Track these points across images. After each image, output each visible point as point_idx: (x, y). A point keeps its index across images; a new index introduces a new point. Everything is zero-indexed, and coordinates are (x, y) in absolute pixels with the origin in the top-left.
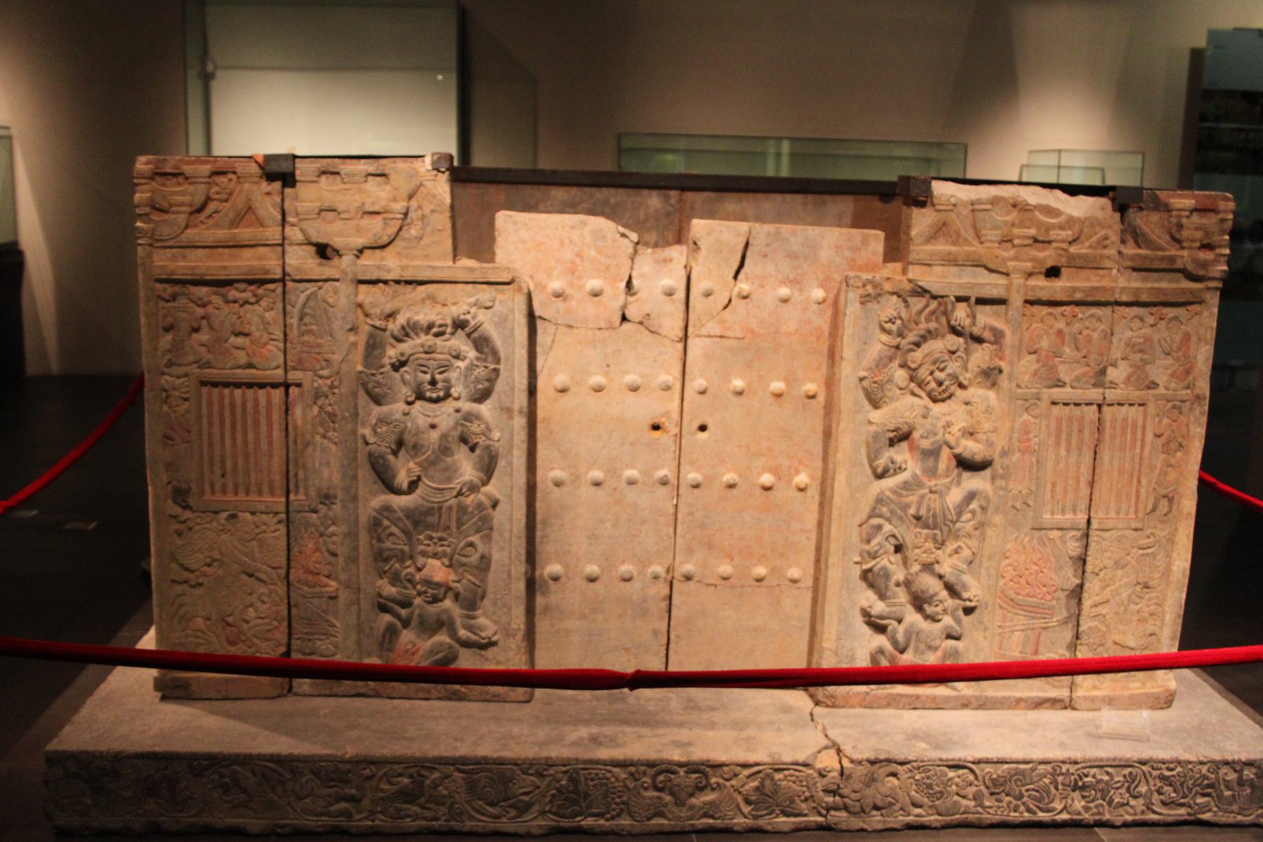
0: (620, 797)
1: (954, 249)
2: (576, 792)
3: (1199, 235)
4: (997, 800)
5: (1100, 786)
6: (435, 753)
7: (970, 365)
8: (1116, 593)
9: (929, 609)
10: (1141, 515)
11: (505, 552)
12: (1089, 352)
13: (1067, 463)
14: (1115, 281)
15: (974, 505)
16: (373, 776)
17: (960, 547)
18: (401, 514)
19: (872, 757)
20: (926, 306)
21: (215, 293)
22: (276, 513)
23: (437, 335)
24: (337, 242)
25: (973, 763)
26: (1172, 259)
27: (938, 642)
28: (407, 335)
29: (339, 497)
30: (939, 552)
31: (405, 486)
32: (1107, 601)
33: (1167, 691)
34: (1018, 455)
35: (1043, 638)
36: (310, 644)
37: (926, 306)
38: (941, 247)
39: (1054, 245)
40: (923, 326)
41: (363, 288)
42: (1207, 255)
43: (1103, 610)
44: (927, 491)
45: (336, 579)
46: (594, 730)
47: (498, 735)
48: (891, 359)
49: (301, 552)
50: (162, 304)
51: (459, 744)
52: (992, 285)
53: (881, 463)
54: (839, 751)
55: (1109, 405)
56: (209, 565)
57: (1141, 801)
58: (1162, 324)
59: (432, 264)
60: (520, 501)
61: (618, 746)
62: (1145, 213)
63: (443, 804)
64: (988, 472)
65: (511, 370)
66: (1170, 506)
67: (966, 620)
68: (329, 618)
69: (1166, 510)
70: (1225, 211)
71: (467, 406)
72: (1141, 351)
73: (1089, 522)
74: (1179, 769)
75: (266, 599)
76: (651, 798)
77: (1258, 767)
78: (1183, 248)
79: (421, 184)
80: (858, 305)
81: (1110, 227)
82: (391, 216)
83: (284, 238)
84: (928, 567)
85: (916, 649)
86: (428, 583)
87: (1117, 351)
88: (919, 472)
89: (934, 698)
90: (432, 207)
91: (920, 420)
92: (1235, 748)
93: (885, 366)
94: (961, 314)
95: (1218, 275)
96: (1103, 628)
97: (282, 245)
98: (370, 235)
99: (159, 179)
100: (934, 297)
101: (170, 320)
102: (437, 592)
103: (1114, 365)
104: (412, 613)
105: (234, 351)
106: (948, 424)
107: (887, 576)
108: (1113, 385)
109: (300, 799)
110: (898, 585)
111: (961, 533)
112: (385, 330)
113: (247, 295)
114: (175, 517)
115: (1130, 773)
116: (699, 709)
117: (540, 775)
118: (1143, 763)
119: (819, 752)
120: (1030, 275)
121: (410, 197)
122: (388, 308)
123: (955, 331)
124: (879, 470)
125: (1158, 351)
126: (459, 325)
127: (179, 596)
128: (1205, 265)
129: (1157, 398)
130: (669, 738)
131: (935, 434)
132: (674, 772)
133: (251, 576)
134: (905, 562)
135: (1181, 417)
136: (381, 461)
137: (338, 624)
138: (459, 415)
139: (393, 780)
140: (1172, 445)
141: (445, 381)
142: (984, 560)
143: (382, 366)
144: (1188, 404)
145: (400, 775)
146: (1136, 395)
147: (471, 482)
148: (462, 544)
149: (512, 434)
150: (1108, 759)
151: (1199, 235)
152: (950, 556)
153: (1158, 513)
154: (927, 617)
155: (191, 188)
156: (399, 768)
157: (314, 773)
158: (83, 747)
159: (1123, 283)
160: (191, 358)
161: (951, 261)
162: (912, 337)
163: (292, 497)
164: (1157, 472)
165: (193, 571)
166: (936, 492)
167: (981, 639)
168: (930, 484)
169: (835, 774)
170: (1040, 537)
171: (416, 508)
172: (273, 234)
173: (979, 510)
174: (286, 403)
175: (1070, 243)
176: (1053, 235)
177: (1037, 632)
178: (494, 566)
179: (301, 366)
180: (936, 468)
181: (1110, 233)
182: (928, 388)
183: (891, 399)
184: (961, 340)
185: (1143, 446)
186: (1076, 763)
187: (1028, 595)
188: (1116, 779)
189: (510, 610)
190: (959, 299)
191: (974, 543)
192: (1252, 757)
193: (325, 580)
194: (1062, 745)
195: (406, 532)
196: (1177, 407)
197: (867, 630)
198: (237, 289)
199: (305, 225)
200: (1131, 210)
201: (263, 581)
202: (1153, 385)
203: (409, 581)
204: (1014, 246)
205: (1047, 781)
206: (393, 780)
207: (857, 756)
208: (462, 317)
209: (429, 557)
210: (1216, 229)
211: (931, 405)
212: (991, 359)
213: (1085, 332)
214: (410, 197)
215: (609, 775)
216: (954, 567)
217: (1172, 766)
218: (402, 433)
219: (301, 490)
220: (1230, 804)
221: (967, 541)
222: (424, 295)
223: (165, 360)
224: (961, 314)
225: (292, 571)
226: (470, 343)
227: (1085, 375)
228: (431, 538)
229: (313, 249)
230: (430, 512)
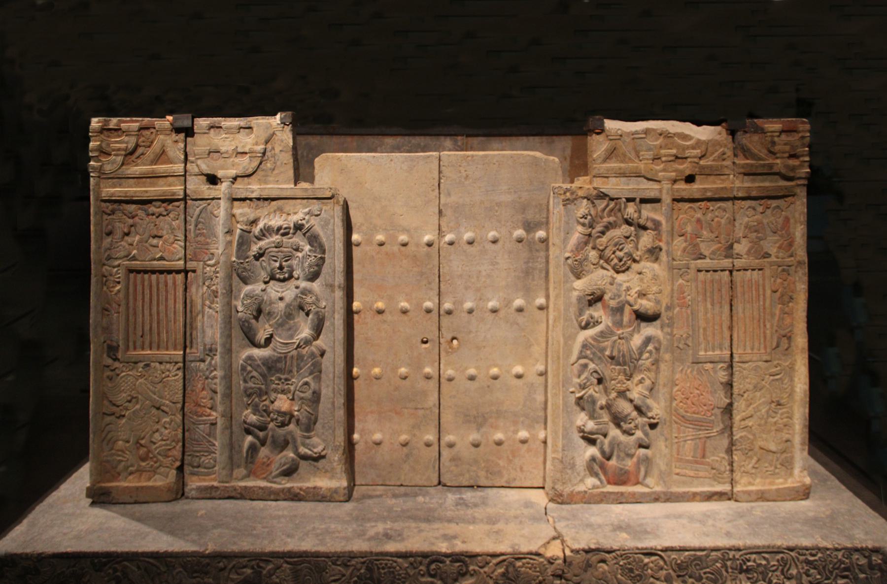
1: (622, 165)
3: (787, 148)
6: (269, 549)
7: (639, 246)
8: (757, 410)
9: (625, 426)
11: (331, 390)
12: (720, 233)
14: (733, 183)
17: (643, 378)
18: (259, 362)
20: (607, 206)
22: (176, 363)
23: (283, 235)
24: (220, 174)
25: (662, 551)
26: (771, 166)
27: (633, 451)
28: (264, 235)
30: (628, 382)
31: (263, 341)
32: (751, 416)
34: (678, 309)
35: (708, 444)
36: (197, 459)
37: (607, 206)
38: (613, 165)
39: (689, 160)
41: (236, 203)
42: (793, 162)
43: (750, 423)
44: (617, 337)
46: (389, 525)
47: (318, 531)
49: (193, 391)
50: (105, 217)
51: (289, 540)
52: (649, 189)
54: (563, 542)
56: (130, 401)
58: (769, 212)
59: (280, 186)
60: (340, 351)
62: (748, 135)
64: (658, 322)
65: (333, 258)
66: (789, 344)
67: (652, 433)
68: (211, 439)
69: (786, 346)
70: (803, 131)
71: (303, 284)
72: (756, 231)
73: (732, 355)
74: (820, 555)
75: (167, 426)
77: (883, 554)
78: (777, 158)
79: (274, 134)
80: (561, 206)
81: (725, 146)
82: (254, 155)
83: (186, 171)
84: (622, 394)
85: (618, 457)
86: (279, 413)
87: (739, 232)
88: (610, 325)
89: (633, 494)
90: (281, 148)
91: (609, 287)
92: (862, 536)
93: (582, 249)
95: (803, 176)
96: (751, 437)
97: (185, 176)
98: (241, 168)
99: (105, 133)
100: (612, 199)
102: (287, 418)
103: (738, 242)
104: (267, 435)
105: (151, 248)
107: (593, 402)
108: (739, 256)
110: (602, 408)
111: (643, 368)
112: (250, 232)
113: (162, 210)
114: (108, 367)
115: (782, 558)
117: (346, 565)
120: (675, 181)
121: (267, 142)
122: (252, 217)
123: (628, 222)
124: (583, 324)
125: (768, 232)
127: (108, 425)
128: (793, 169)
129: (771, 264)
130: (441, 532)
131: (619, 296)
132: (442, 562)
133: (158, 409)
134: (606, 391)
135: (790, 278)
137: (217, 444)
138: (298, 291)
139: (240, 571)
141: (289, 266)
142: (661, 387)
144: (793, 268)
145: (245, 567)
146: (756, 262)
147: (306, 337)
148: (300, 384)
149: (334, 303)
150: (764, 547)
151: (787, 148)
152: (637, 385)
153: (780, 349)
154: (625, 432)
156: (243, 561)
157: (182, 567)
159: (737, 184)
160: (122, 254)
161: (622, 174)
162: (599, 228)
163: (188, 351)
164: (776, 318)
165: (118, 406)
167: (663, 447)
168: (619, 332)
169: (560, 561)
170: (698, 369)
171: (270, 357)
172: (179, 168)
173: (654, 351)
174: (186, 284)
176: (688, 153)
177: (703, 440)
178: (322, 399)
179: (195, 258)
180: (622, 320)
182: (613, 263)
183: (588, 272)
184: (632, 228)
185: (764, 300)
186: (739, 550)
187: (694, 413)
188: (772, 563)
189: (334, 431)
190: (629, 200)
193: (209, 411)
194: (728, 534)
195: (264, 376)
197: (582, 443)
198: (155, 206)
199: (199, 162)
200: (739, 133)
201: (167, 413)
202: (767, 255)
203: (265, 411)
205: (719, 565)
206: (240, 571)
207: (576, 546)
209: (279, 393)
210: (798, 143)
211: (615, 275)
212: (654, 241)
213: (716, 219)
214: (267, 142)
215: (395, 564)
216: (640, 394)
217: (814, 552)
218: (260, 304)
219: (195, 346)
225: (186, 404)
226: (306, 240)
227: (718, 249)
228: (280, 379)
230: (279, 360)
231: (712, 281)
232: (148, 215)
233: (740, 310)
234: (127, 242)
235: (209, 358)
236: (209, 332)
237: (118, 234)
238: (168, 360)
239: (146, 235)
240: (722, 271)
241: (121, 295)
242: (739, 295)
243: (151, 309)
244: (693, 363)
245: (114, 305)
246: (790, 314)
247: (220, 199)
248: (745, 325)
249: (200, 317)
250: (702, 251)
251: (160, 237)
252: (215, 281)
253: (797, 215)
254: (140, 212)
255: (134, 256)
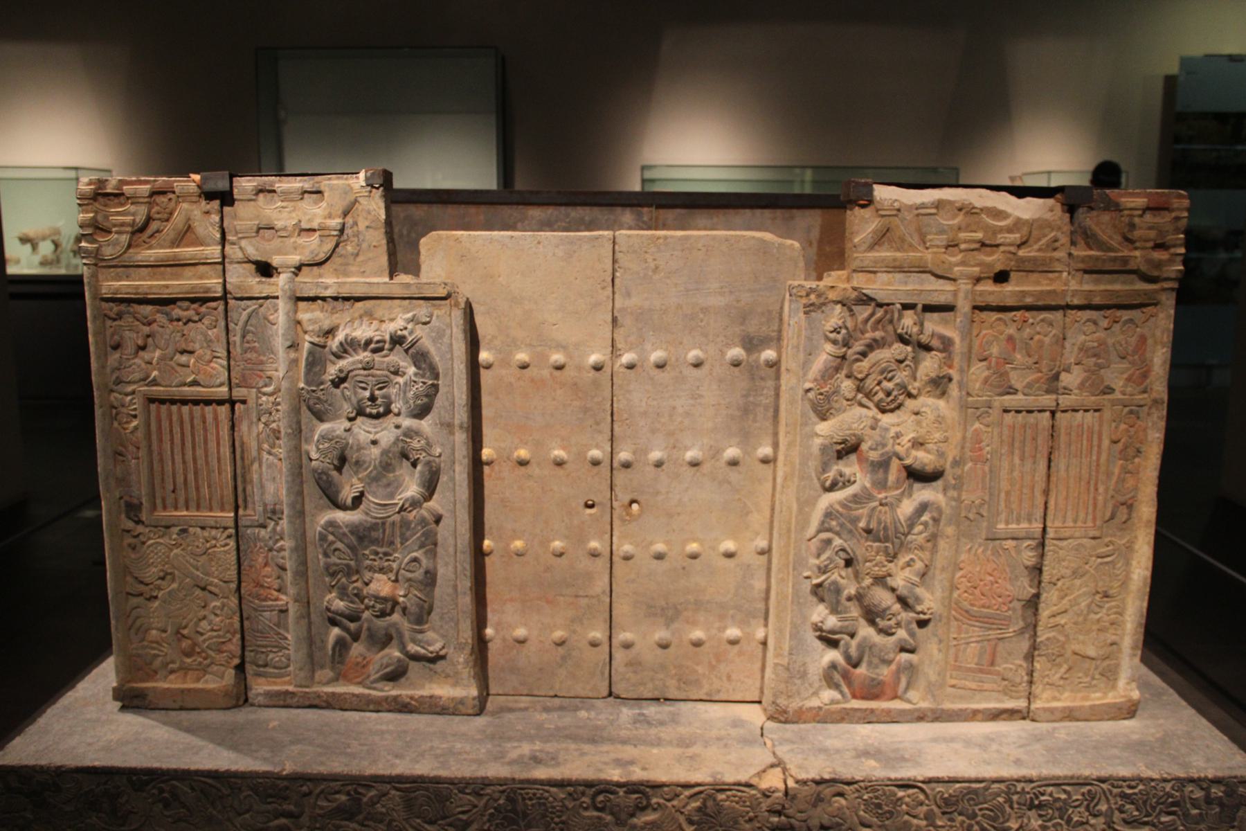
0: (559, 817)
1: (898, 255)
2: (514, 811)
4: (950, 820)
5: (1058, 805)
7: (918, 375)
8: (1075, 603)
9: (882, 623)
10: (1098, 523)
12: (1041, 357)
13: (1021, 472)
15: (926, 517)
16: (310, 793)
17: (912, 560)
18: (346, 530)
19: (818, 778)
21: (158, 312)
22: (226, 528)
23: (375, 351)
24: (276, 261)
25: (923, 782)
26: (1125, 260)
27: (891, 656)
28: (346, 351)
29: (286, 512)
31: (349, 501)
32: (1065, 612)
33: (1130, 701)
35: (1000, 648)
36: (263, 656)
38: (885, 253)
39: (1002, 249)
40: (869, 335)
41: (302, 304)
45: (286, 594)
46: (538, 746)
47: (439, 752)
48: (837, 369)
49: (251, 567)
50: (109, 323)
51: (397, 761)
52: (938, 291)
53: (831, 475)
54: (784, 770)
55: (1063, 411)
56: (163, 578)
57: (1101, 820)
58: (1116, 327)
59: (368, 280)
61: (558, 764)
62: (1094, 213)
63: (381, 822)
64: (939, 484)
65: (451, 385)
66: (1130, 514)
67: (921, 633)
68: (282, 631)
71: (407, 422)
72: (1095, 355)
73: (1044, 529)
74: (1141, 787)
75: (218, 612)
76: (591, 818)
78: (1136, 249)
79: (356, 201)
80: (801, 315)
81: (1059, 228)
83: (224, 257)
84: (880, 580)
85: (870, 663)
86: (377, 598)
87: (1070, 356)
88: (868, 485)
89: (889, 712)
90: (367, 223)
91: (868, 431)
92: (1202, 764)
93: (831, 377)
94: (908, 321)
95: (1173, 275)
96: (1062, 638)
97: (223, 263)
98: (307, 252)
99: (101, 199)
100: (880, 305)
101: (116, 338)
102: (389, 606)
103: (1068, 370)
104: (361, 627)
105: (178, 369)
106: (898, 436)
107: (838, 590)
108: (1067, 391)
109: (240, 815)
110: (849, 599)
112: (324, 347)
113: (191, 313)
114: (128, 531)
115: (1089, 791)
116: (649, 723)
117: (478, 794)
118: (1102, 780)
119: (764, 771)
120: (978, 280)
121: (345, 214)
122: (326, 325)
123: (903, 340)
124: (828, 484)
125: (1114, 357)
126: (397, 340)
128: (1159, 265)
129: (1114, 403)
130: (613, 756)
131: (884, 445)
132: (612, 793)
133: (204, 589)
135: (1139, 423)
136: (325, 477)
137: (289, 637)
139: (330, 797)
140: (1130, 451)
141: (384, 397)
142: (937, 572)
143: (322, 383)
144: (1146, 409)
145: (338, 792)
147: (413, 497)
148: (406, 560)
149: (453, 450)
150: (1066, 777)
151: (1152, 234)
152: (903, 568)
153: (1116, 521)
154: (881, 631)
155: (132, 208)
157: (252, 789)
158: (25, 762)
159: (1073, 286)
160: (137, 376)
162: (858, 347)
163: (241, 512)
164: (1115, 478)
166: (886, 504)
168: (880, 496)
169: (780, 794)
170: (994, 547)
171: (361, 524)
172: (213, 251)
173: (931, 522)
174: (232, 420)
175: (1019, 246)
176: (1000, 238)
177: (993, 643)
178: (439, 581)
179: (245, 383)
180: (886, 479)
181: (1059, 234)
182: (876, 398)
183: (838, 410)
184: (909, 349)
185: (1099, 453)
186: (1031, 781)
187: (983, 606)
190: (906, 307)
191: (926, 555)
192: (1220, 774)
194: (1018, 762)
196: (1134, 412)
197: (819, 645)
198: (180, 307)
200: (1081, 210)
202: (1109, 390)
203: (356, 595)
204: (961, 251)
205: (1001, 800)
206: (330, 797)
208: (399, 333)
209: (375, 571)
211: (880, 416)
212: (940, 367)
213: (1037, 337)
214: (345, 214)
215: (546, 795)
216: (907, 580)
217: (1133, 783)
218: (343, 450)
219: (250, 505)
220: (1197, 823)
221: (920, 553)
222: (362, 312)
223: (114, 377)
224: (908, 321)
225: (243, 584)
226: (409, 359)
227: (1037, 381)
228: (377, 553)
229: (253, 267)
230: (374, 527)
231: (1024, 426)
232: (171, 321)
233: (1062, 467)
234: (142, 358)
235: (273, 523)
236: (270, 488)
237: (129, 348)
238: (213, 524)
239: (170, 350)
240: (1040, 411)
241: (140, 434)
242: (1062, 446)
243: (183, 454)
244: (987, 539)
245: (131, 448)
246: (1135, 473)
247: (277, 298)
248: (1068, 488)
249: (256, 466)
250: (1013, 382)
251: (192, 352)
252: (276, 416)
253: (1158, 333)
254: (159, 317)
255: (154, 380)
